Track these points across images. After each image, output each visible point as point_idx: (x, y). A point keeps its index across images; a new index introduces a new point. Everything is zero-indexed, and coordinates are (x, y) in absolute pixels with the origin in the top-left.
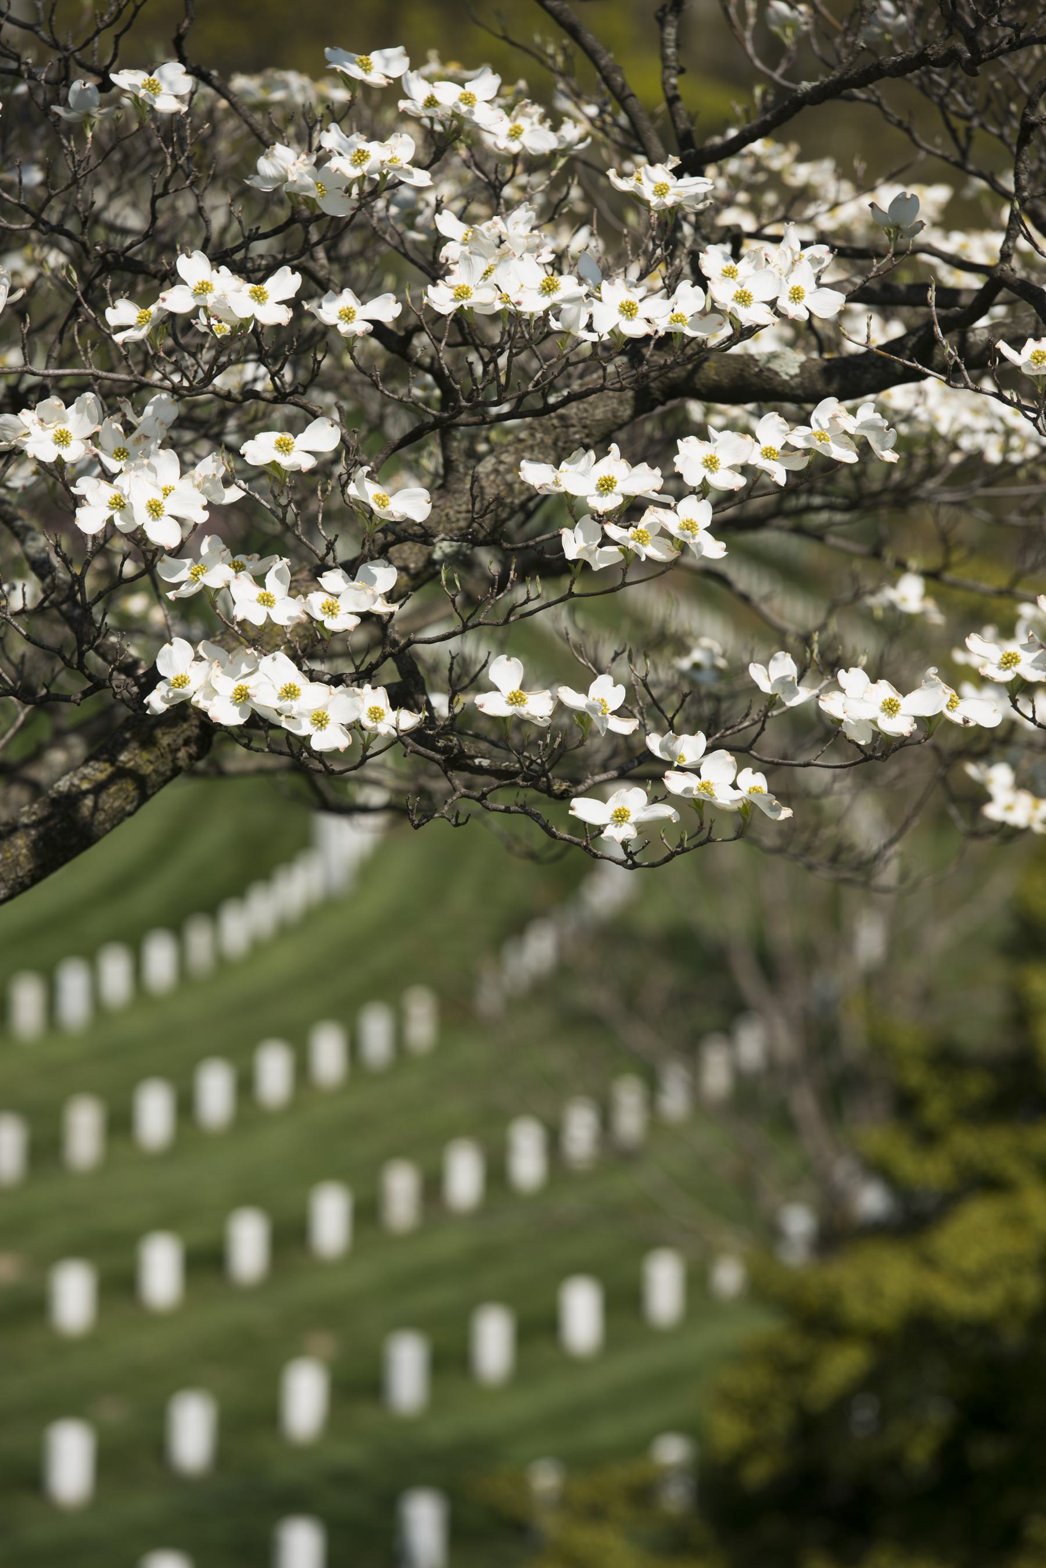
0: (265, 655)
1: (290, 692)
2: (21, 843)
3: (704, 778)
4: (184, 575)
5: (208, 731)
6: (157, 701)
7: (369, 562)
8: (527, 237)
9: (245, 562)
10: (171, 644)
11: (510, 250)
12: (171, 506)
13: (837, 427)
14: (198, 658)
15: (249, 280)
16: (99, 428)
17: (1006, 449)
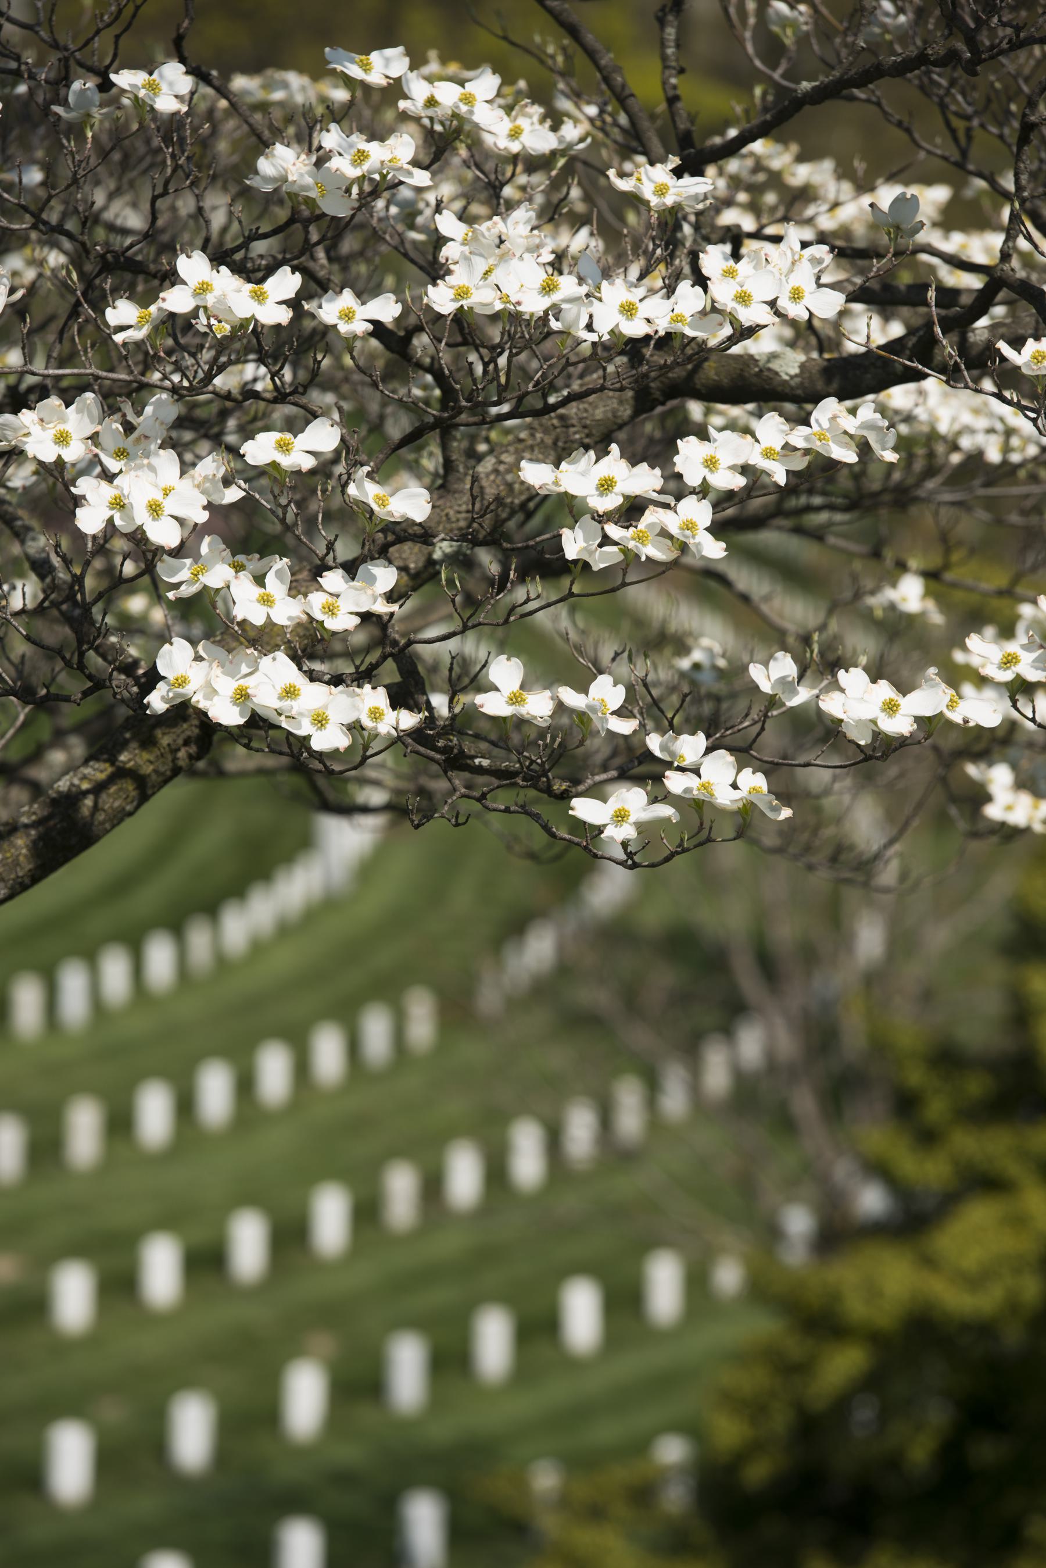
0: (265, 655)
1: (290, 692)
2: (21, 843)
3: (704, 778)
4: (184, 575)
5: (208, 731)
6: (157, 701)
7: (369, 562)
8: (527, 237)
9: (245, 562)
10: (171, 644)
11: (510, 250)
12: (171, 506)
13: (837, 427)
14: (198, 658)
15: (249, 280)
16: (99, 428)
17: (1006, 449)
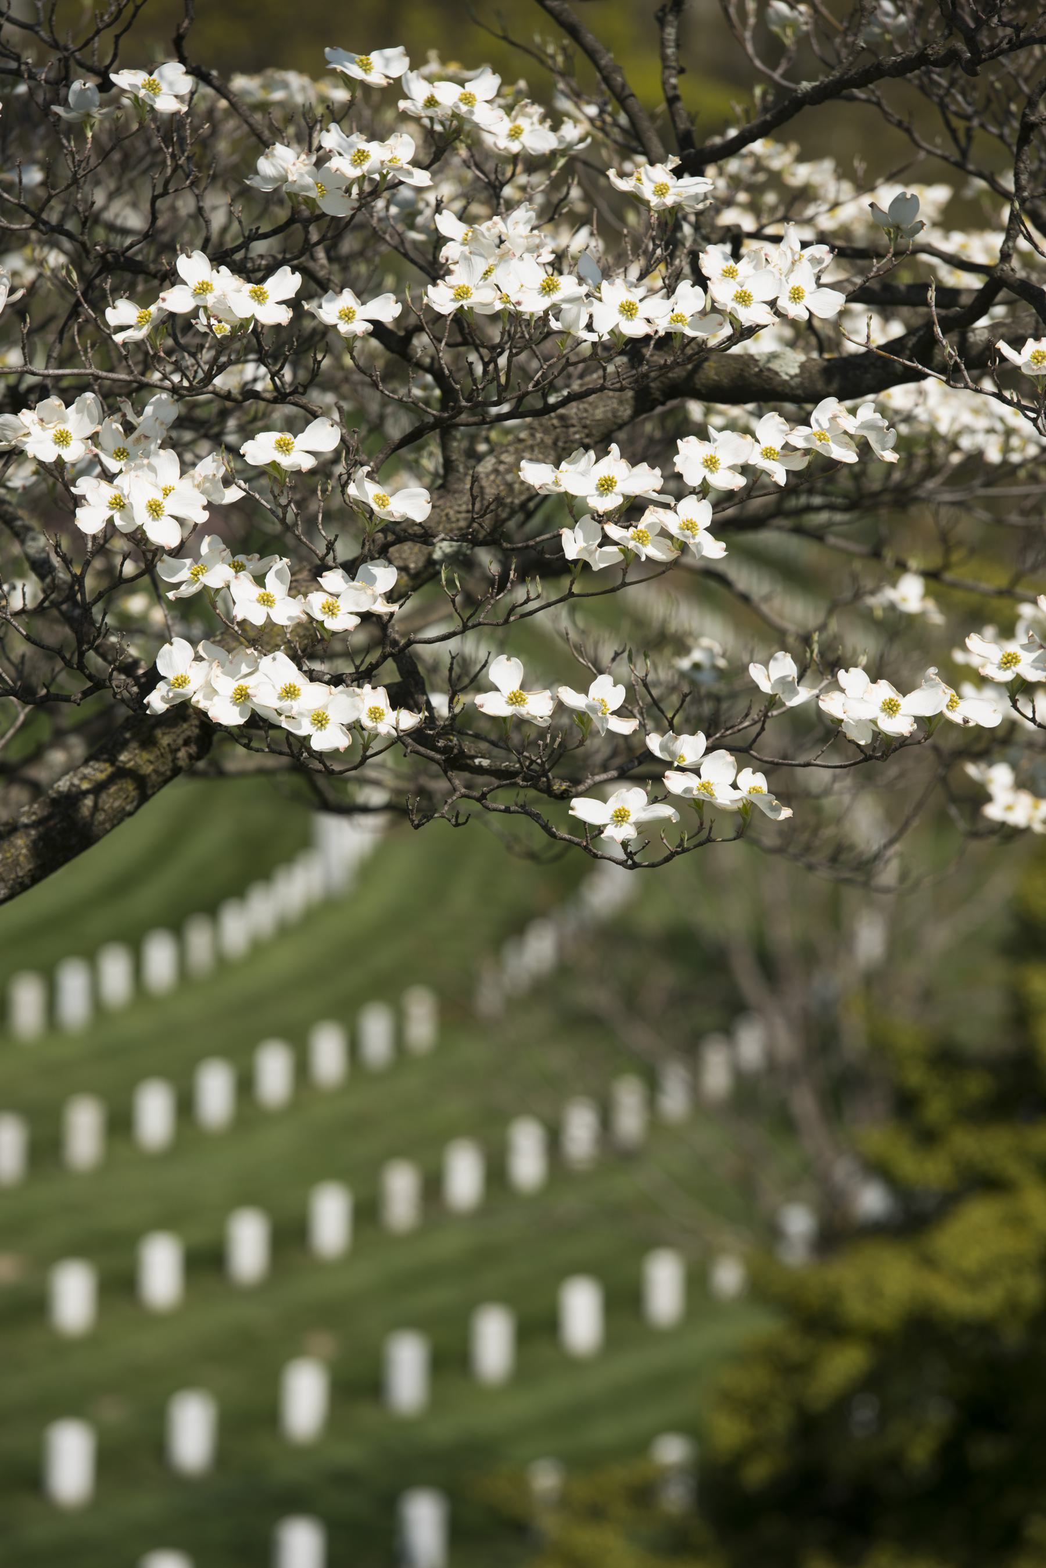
0: (265, 655)
1: (290, 692)
2: (21, 843)
3: (704, 778)
4: (184, 575)
5: (208, 731)
6: (157, 701)
7: (369, 562)
8: (527, 237)
9: (245, 562)
10: (171, 644)
11: (510, 250)
12: (171, 506)
13: (837, 427)
14: (198, 658)
15: (249, 280)
16: (99, 428)
17: (1006, 449)
